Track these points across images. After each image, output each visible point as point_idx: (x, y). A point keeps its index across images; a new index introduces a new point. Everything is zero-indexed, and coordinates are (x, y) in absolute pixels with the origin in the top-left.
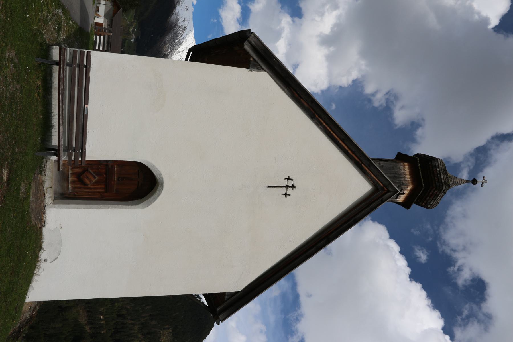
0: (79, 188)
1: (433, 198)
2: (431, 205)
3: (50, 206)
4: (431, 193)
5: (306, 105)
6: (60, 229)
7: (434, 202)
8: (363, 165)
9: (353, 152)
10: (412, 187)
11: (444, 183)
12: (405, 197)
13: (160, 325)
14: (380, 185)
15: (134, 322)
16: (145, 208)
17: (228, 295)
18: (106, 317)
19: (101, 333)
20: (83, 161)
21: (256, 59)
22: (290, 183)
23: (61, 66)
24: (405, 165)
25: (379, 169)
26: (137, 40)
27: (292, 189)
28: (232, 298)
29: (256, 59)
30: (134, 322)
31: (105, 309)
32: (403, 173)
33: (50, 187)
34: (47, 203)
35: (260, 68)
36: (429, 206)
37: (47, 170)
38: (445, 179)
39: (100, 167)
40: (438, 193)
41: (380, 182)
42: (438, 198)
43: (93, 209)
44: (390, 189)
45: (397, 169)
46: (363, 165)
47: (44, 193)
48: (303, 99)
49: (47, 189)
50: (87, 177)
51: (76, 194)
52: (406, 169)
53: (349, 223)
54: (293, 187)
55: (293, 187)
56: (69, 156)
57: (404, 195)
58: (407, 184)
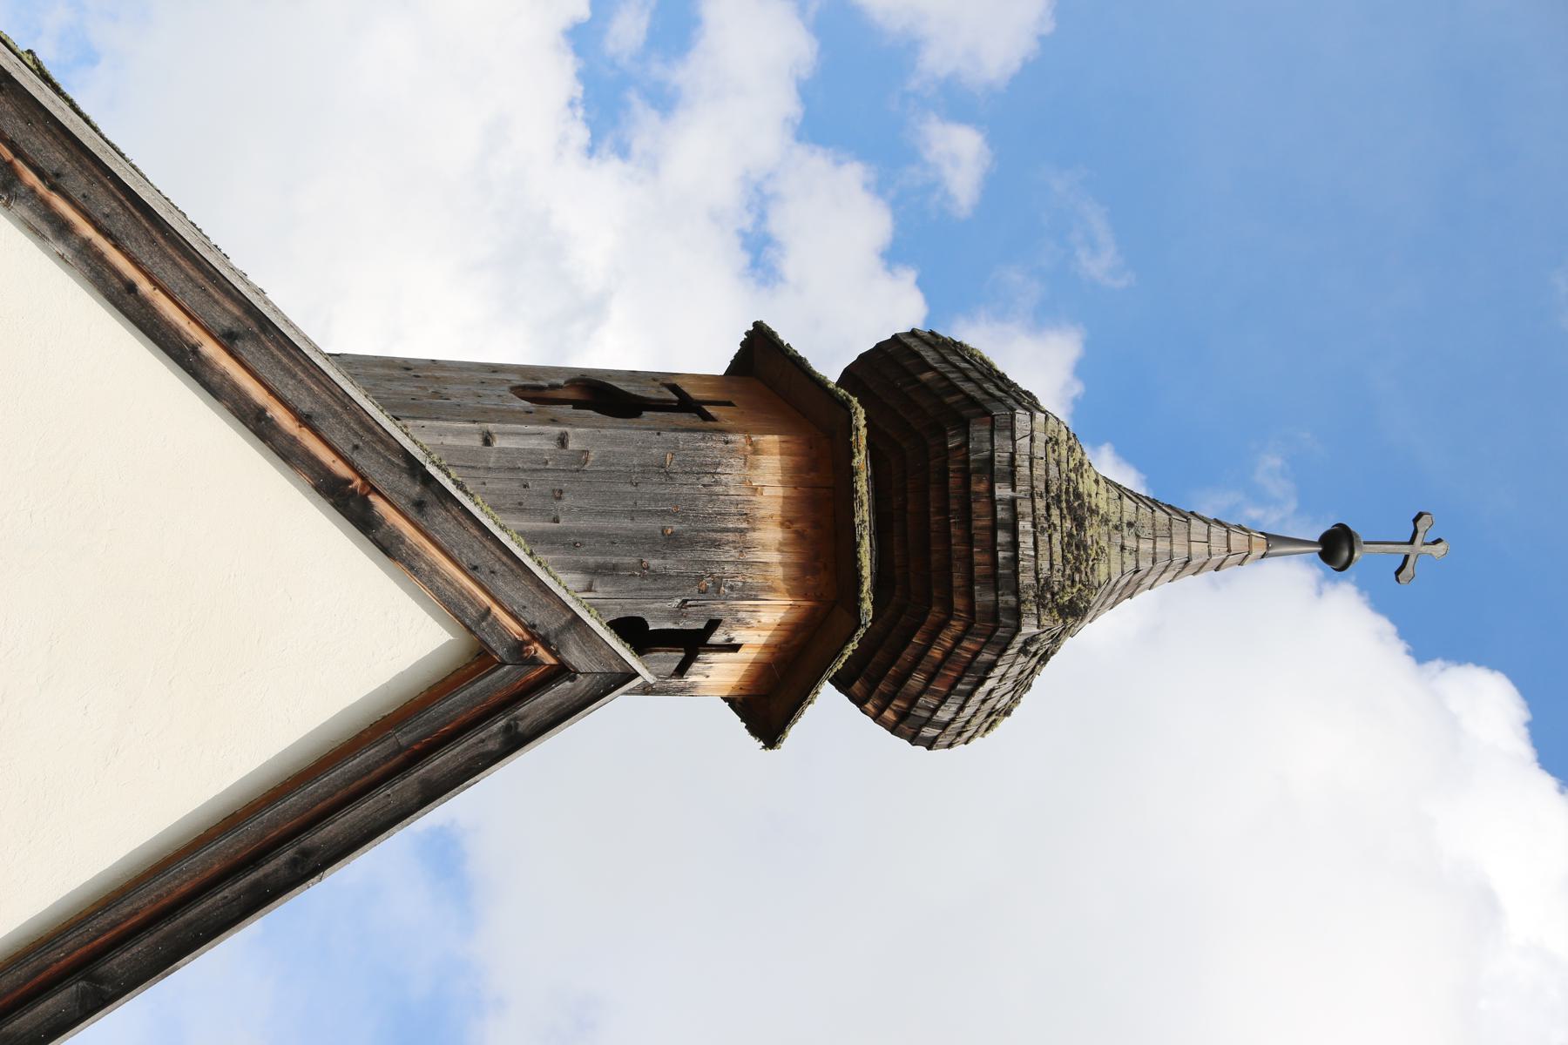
1: (953, 687)
4: (936, 653)
7: (961, 708)
8: (372, 498)
12: (746, 666)
24: (756, 452)
32: (733, 510)
36: (928, 732)
38: (1044, 565)
40: (986, 656)
44: (575, 656)
45: (693, 479)
57: (731, 655)
58: (749, 593)
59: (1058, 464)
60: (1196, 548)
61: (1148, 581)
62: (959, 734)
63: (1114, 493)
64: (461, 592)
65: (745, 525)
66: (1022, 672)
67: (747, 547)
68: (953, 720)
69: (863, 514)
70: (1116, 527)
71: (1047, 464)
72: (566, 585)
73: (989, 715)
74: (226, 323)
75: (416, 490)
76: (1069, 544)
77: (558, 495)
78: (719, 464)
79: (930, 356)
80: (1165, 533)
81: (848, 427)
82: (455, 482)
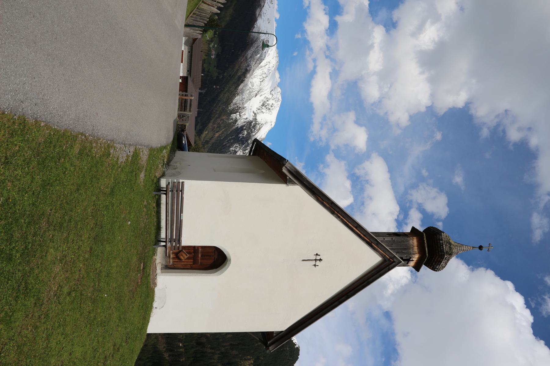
0: (177, 262)
2: (437, 269)
4: (436, 260)
5: (327, 205)
6: (165, 289)
8: (372, 244)
9: (364, 235)
10: (419, 256)
11: (445, 253)
14: (387, 257)
15: (214, 351)
17: (275, 333)
18: (185, 344)
19: (180, 361)
20: (180, 246)
22: (318, 258)
24: (413, 239)
26: (217, 55)
30: (214, 351)
31: (184, 336)
35: (293, 183)
38: (447, 249)
40: (441, 260)
42: (442, 263)
44: (395, 260)
46: (372, 244)
48: (325, 202)
49: (158, 264)
50: (182, 255)
51: (175, 266)
52: (414, 242)
53: (363, 285)
54: (320, 260)
55: (320, 260)
56: (172, 244)
58: (414, 254)
60: (464, 248)
67: (413, 249)
69: (426, 245)
75: (376, 242)
77: (392, 244)
79: (432, 229)
81: (423, 236)
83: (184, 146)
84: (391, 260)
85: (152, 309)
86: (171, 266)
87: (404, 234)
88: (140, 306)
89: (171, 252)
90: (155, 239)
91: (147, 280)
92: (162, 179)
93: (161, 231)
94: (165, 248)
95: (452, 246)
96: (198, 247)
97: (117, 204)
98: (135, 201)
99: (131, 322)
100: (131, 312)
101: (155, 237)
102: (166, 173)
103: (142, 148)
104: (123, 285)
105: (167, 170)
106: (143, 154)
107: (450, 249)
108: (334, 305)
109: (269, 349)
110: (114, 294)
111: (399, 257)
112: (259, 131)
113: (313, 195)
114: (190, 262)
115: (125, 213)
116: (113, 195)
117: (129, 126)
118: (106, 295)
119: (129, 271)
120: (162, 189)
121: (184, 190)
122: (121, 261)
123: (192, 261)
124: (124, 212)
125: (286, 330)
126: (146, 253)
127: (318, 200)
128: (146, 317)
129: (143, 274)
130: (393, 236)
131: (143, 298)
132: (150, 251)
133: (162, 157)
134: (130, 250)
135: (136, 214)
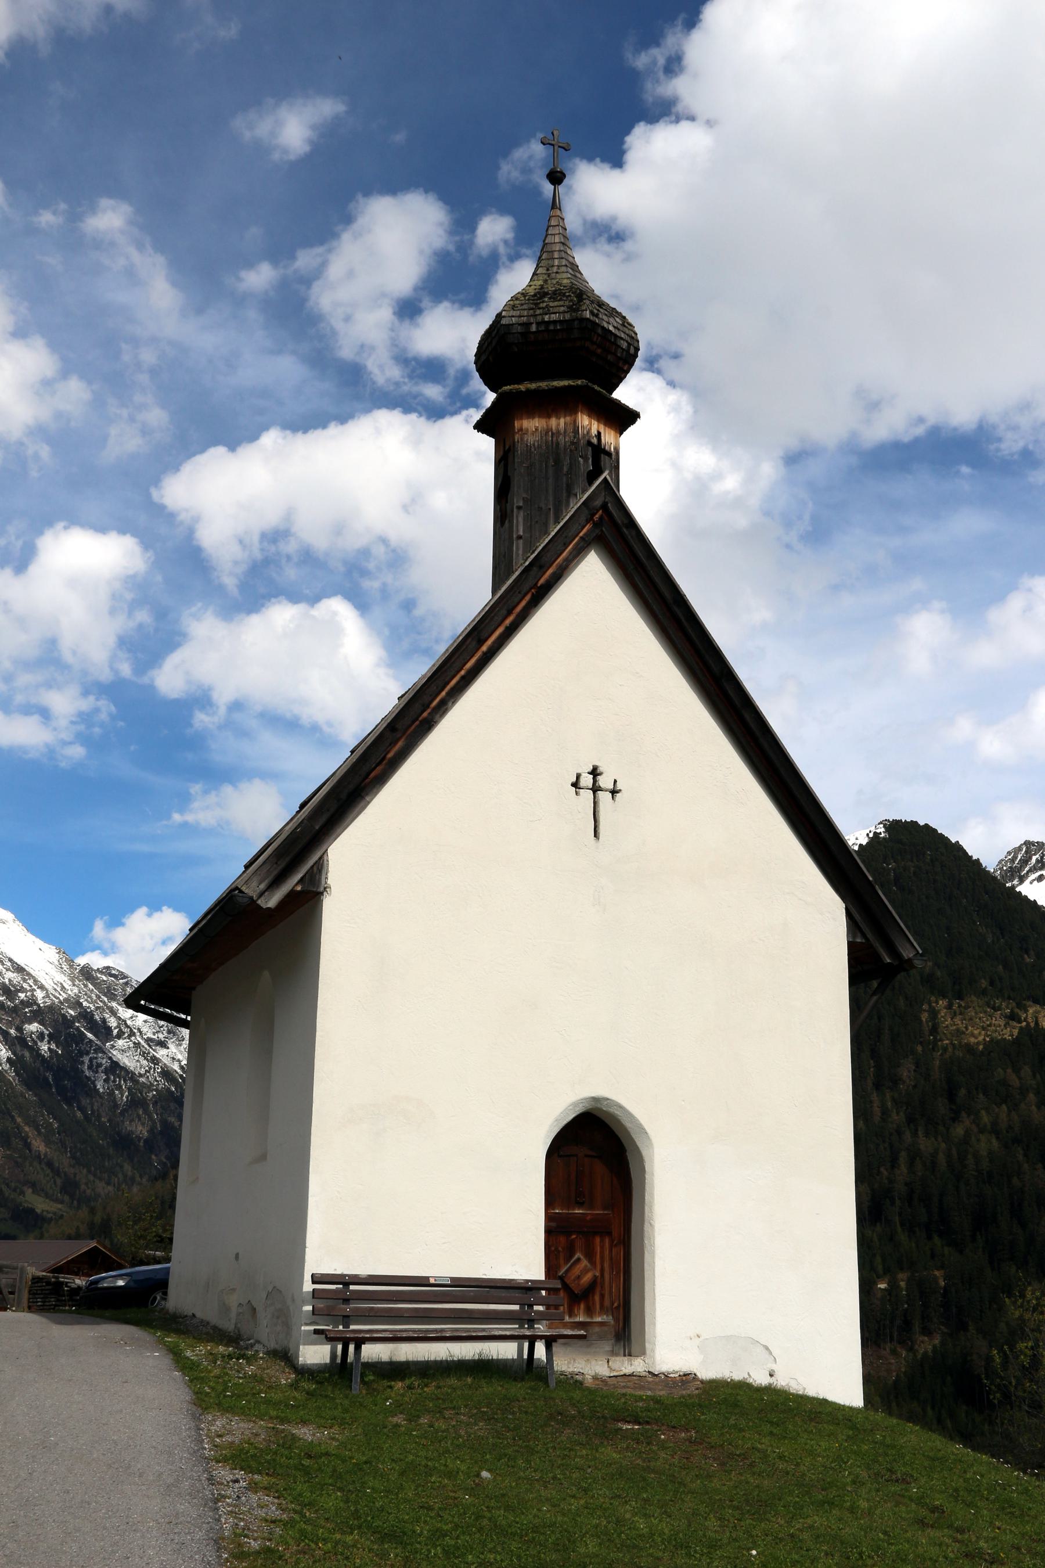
0: (602, 1296)
2: (629, 344)
3: (651, 1363)
4: (599, 351)
6: (701, 1339)
7: (622, 338)
8: (539, 585)
13: (919, 1048)
16: (652, 1145)
21: (299, 876)
22: (587, 780)
23: (349, 1338)
24: (521, 429)
25: (551, 536)
27: (600, 774)
28: (861, 926)
29: (299, 876)
30: (903, 1154)
32: (544, 438)
33: (608, 1362)
34: (643, 1370)
35: (319, 869)
37: (571, 1370)
38: (562, 309)
39: (553, 1249)
40: (600, 331)
41: (580, 532)
42: (611, 328)
43: (654, 1263)
44: (598, 503)
47: (622, 1376)
48: (388, 752)
50: (579, 1278)
51: (616, 1305)
54: (595, 772)
55: (595, 772)
56: (541, 1317)
58: (576, 430)
59: (522, 305)
60: (557, 240)
61: (571, 259)
62: (633, 338)
63: (535, 277)
64: (574, 549)
65: (550, 433)
66: (606, 315)
67: (558, 432)
68: (627, 342)
69: (543, 385)
70: (549, 276)
71: (521, 310)
72: (575, 505)
73: (625, 326)
74: (474, 643)
75: (535, 569)
76: (554, 298)
77: (540, 509)
78: (527, 445)
79: (484, 357)
80: (551, 254)
81: (510, 392)
82: (532, 554)
83: (136, 1281)
84: (596, 517)
85: (779, 1390)
86: (617, 1320)
87: (502, 463)
88: (771, 1433)
89: (567, 1319)
90: (522, 1379)
91: (677, 1409)
92: (300, 1359)
93: (495, 1357)
94: (555, 1341)
95: (550, 288)
96: (549, 1218)
97: (431, 1517)
98: (402, 1457)
99: (833, 1465)
100: (798, 1465)
101: (515, 1380)
102: (272, 1345)
103: (207, 1436)
104: (707, 1493)
105: (258, 1342)
106: (230, 1432)
107: (560, 294)
108: (753, 725)
109: (910, 960)
110: (742, 1523)
111: (587, 490)
112: (29, 974)
113: (363, 798)
114: (602, 1247)
115: (455, 1492)
116: (405, 1533)
117: (143, 1487)
118: (754, 1552)
119: (654, 1471)
120: (339, 1360)
121: (343, 1276)
122: (626, 1502)
123: (598, 1240)
124: (452, 1494)
125: (843, 898)
126: (579, 1412)
127: (382, 779)
128: (810, 1411)
129: (657, 1421)
130: (508, 505)
131: (742, 1423)
132: (572, 1398)
133: (216, 1363)
134: (580, 1469)
135: (447, 1451)
